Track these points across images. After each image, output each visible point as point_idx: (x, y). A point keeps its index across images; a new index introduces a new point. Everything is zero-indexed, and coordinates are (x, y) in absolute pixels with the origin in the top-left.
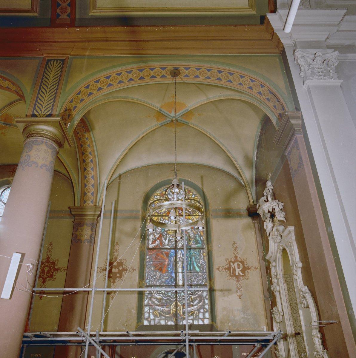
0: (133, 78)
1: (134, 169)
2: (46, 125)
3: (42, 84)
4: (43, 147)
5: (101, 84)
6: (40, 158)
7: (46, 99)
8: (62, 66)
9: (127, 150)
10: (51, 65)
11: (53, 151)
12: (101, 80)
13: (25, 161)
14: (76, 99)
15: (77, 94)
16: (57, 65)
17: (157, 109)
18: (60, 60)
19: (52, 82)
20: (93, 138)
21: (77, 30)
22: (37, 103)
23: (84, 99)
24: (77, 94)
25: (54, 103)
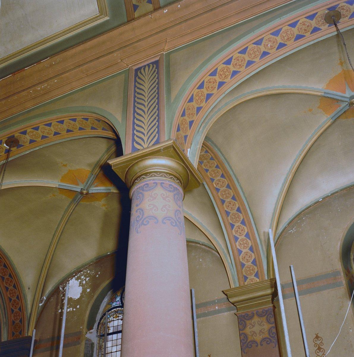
0: (266, 51)
1: (310, 206)
2: (155, 158)
3: (136, 104)
4: (159, 191)
5: (221, 75)
6: (157, 208)
7: (146, 122)
8: (156, 70)
9: (291, 177)
10: (142, 74)
11: (175, 195)
12: (218, 70)
13: (138, 219)
14: (189, 109)
15: (189, 102)
16: (149, 72)
17: (320, 94)
18: (153, 63)
19: (149, 96)
20: (231, 173)
21: (165, 11)
22: (135, 132)
23: (201, 107)
24: (189, 102)
25: (159, 124)
